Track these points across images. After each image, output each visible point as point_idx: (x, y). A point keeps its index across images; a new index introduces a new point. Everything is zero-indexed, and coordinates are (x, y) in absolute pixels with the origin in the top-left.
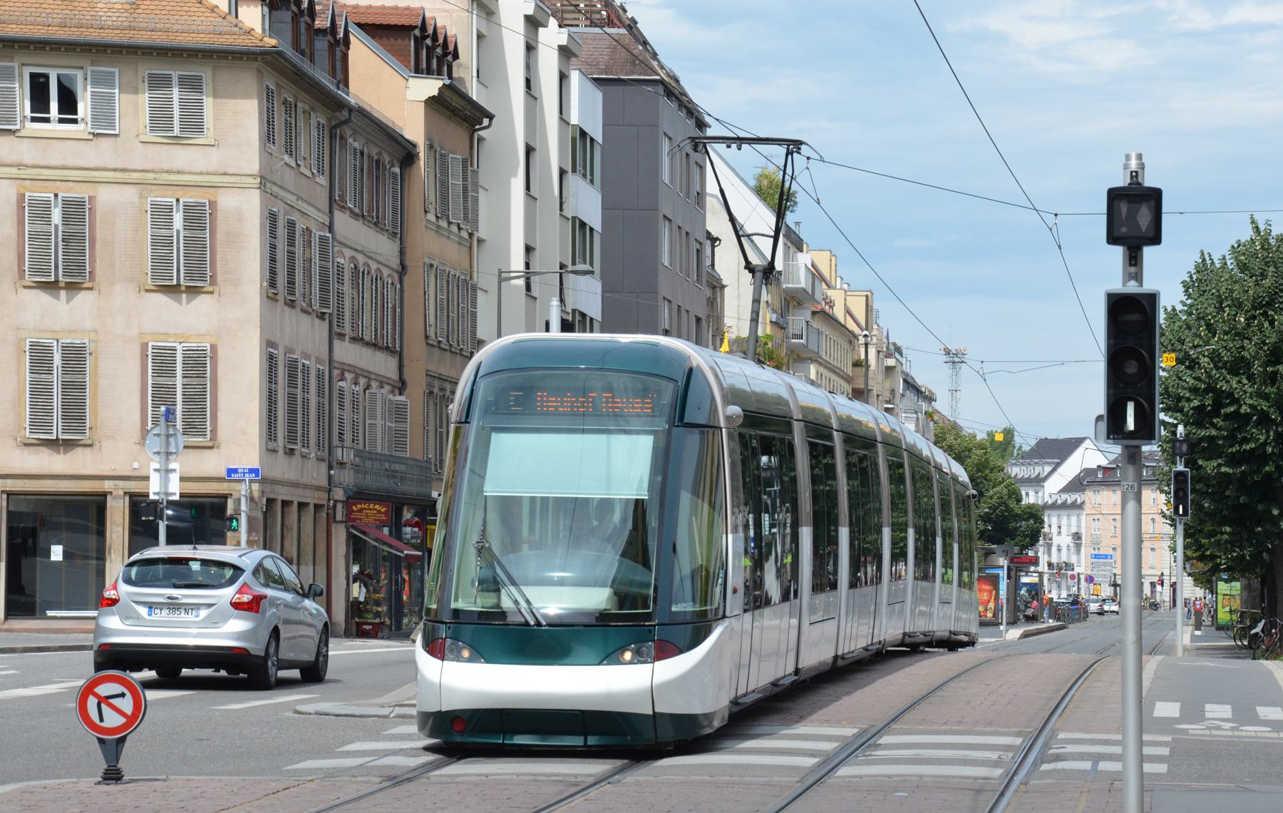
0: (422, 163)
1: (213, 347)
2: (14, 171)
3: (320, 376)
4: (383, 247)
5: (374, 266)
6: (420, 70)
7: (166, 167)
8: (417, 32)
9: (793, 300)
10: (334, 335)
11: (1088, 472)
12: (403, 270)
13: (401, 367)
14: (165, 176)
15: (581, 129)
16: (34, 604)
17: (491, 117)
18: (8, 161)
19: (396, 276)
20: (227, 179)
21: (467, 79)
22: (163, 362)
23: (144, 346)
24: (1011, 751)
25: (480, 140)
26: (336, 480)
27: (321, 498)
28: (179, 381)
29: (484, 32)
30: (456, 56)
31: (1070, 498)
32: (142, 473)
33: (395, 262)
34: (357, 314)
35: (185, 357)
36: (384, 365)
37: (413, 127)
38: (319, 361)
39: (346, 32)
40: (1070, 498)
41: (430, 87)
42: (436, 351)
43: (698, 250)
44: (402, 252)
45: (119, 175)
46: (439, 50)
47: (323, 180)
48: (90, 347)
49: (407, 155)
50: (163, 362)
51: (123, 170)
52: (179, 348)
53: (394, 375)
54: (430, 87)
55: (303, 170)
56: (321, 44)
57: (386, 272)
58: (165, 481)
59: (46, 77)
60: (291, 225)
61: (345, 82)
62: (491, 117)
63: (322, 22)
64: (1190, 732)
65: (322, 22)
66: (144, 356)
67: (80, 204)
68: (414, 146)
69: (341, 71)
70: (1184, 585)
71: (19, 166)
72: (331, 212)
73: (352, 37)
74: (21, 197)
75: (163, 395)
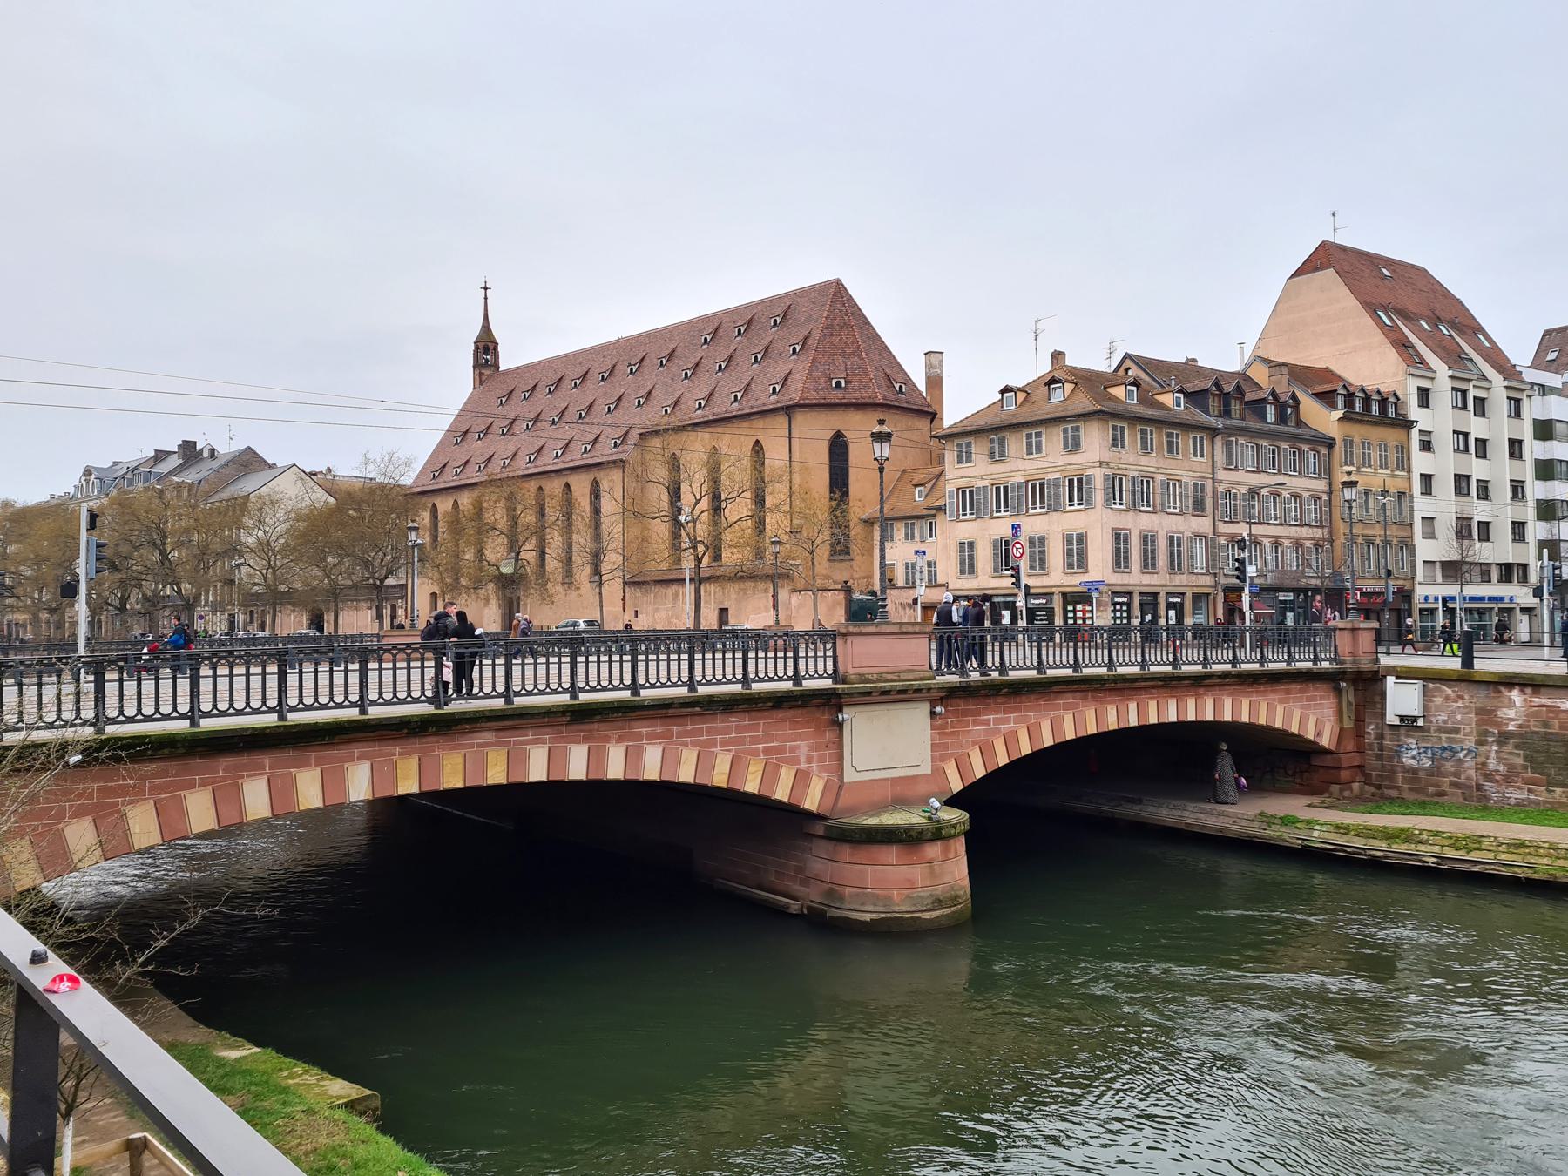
15: (1293, 276)
28: (1075, 547)
68: (1334, 439)
71: (1025, 470)
75: (1069, 554)
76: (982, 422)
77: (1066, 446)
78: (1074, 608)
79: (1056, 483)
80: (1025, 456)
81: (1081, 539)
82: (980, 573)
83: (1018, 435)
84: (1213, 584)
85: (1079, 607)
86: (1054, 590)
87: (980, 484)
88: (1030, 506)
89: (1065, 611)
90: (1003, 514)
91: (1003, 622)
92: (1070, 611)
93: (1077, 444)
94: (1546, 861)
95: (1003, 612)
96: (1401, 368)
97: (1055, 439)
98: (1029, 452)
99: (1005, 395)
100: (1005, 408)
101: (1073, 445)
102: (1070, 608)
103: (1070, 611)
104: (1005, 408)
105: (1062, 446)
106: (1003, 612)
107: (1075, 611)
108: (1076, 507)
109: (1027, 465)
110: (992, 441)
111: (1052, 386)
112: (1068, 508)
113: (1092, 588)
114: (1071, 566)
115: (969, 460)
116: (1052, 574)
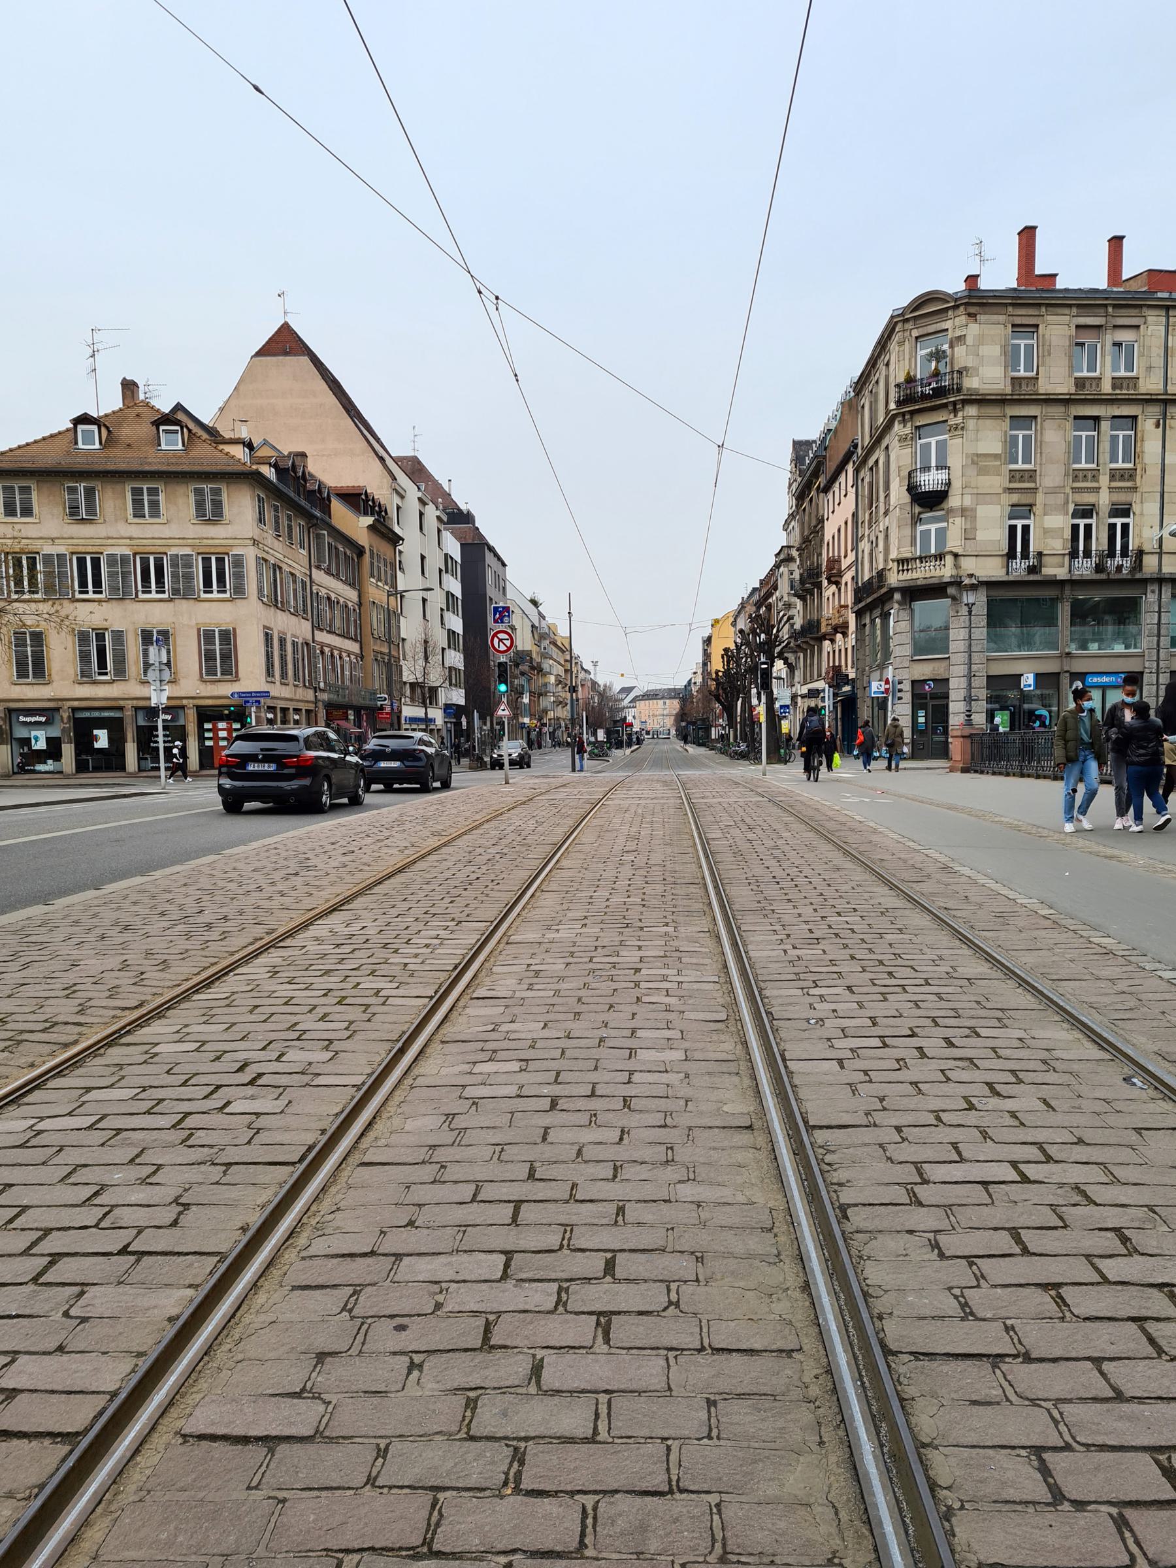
1: (234, 629)
2: (128, 542)
4: (352, 595)
5: (342, 600)
6: (366, 514)
7: (205, 536)
8: (363, 497)
9: (543, 637)
10: (316, 627)
11: (637, 697)
12: (360, 605)
13: (361, 648)
14: (205, 541)
15: (259, 353)
16: (995, 627)
17: (403, 540)
18: (125, 536)
19: (357, 607)
20: (237, 541)
22: (208, 637)
23: (199, 630)
25: (400, 552)
26: (319, 697)
27: (311, 707)
28: (218, 647)
29: (400, 505)
31: (632, 705)
32: (148, 695)
33: (356, 599)
34: (332, 619)
35: (220, 635)
36: (354, 647)
37: (363, 538)
40: (632, 705)
41: (369, 520)
42: (379, 641)
43: (398, 508)
45: (181, 541)
46: (377, 508)
48: (171, 631)
49: (360, 551)
50: (208, 637)
51: (184, 538)
52: (217, 630)
53: (358, 652)
54: (369, 520)
57: (350, 604)
58: (159, 697)
61: (330, 517)
62: (403, 540)
66: (199, 635)
68: (363, 547)
71: (131, 538)
75: (209, 655)
76: (49, 459)
77: (200, 511)
78: (215, 726)
79: (187, 560)
80: (131, 519)
81: (228, 637)
82: (54, 676)
83: (118, 487)
84: (313, 699)
85: (222, 725)
86: (185, 702)
87: (48, 549)
88: (140, 587)
89: (201, 731)
90: (215, 595)
91: (97, 745)
92: (209, 730)
93: (218, 511)
94: (766, 953)
95: (96, 732)
96: (385, 480)
97: (181, 501)
98: (138, 512)
99: (80, 427)
100: (163, 447)
101: (210, 512)
102: (208, 726)
103: (209, 730)
104: (81, 446)
105: (193, 511)
106: (96, 732)
107: (215, 730)
108: (154, 595)
109: (134, 531)
110: (73, 491)
111: (162, 428)
112: (203, 596)
113: (251, 700)
114: (211, 671)
115: (27, 511)
116: (182, 682)
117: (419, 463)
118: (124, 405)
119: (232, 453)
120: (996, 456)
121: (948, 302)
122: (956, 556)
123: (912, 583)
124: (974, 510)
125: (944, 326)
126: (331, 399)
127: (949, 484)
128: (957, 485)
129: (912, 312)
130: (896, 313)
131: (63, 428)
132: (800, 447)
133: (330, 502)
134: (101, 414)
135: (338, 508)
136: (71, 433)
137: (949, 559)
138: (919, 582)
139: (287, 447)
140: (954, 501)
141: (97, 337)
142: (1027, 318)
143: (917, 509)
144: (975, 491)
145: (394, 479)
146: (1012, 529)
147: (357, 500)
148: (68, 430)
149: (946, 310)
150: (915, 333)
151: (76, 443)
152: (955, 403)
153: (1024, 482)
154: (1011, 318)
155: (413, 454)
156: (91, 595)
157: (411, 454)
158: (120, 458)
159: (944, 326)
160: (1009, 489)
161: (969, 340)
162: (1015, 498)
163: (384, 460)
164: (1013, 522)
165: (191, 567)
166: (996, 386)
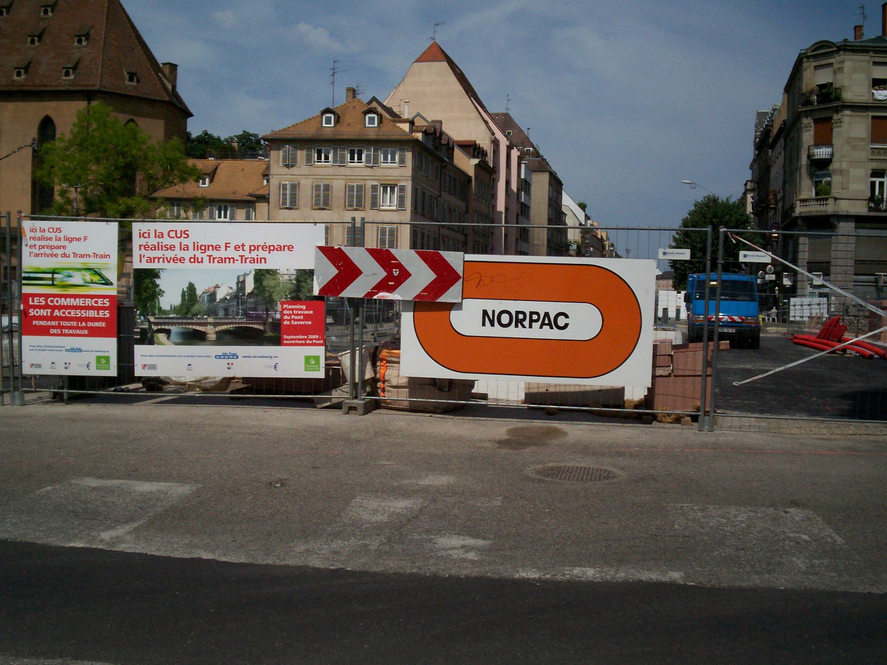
0: (473, 182)
2: (344, 177)
3: (435, 238)
6: (474, 157)
21: (489, 161)
24: (50, 309)
28: (387, 237)
30: (487, 156)
37: (471, 172)
38: (434, 233)
39: (453, 146)
41: (476, 161)
44: (467, 207)
47: (438, 182)
49: (469, 179)
54: (476, 161)
55: (430, 178)
56: (444, 148)
59: (31, 44)
60: (424, 194)
63: (444, 142)
64: (304, 307)
65: (444, 142)
67: (361, 186)
68: (471, 177)
69: (451, 158)
70: (356, 233)
71: (346, 176)
72: (440, 192)
73: (455, 148)
74: (346, 185)
104: (324, 125)
106: (54, 315)
117: (511, 118)
118: (347, 101)
119: (401, 127)
120: (863, 139)
121: (832, 47)
122: (836, 199)
123: (808, 214)
124: (848, 171)
125: (831, 61)
126: (458, 87)
127: (832, 155)
128: (837, 156)
129: (813, 51)
130: (803, 52)
131: (315, 115)
132: (761, 115)
133: (453, 150)
134: (335, 107)
135: (458, 154)
136: (319, 119)
137: (831, 201)
138: (813, 214)
139: (431, 116)
140: (834, 166)
141: (337, 65)
142: (882, 58)
143: (813, 169)
144: (848, 160)
145: (493, 134)
146: (873, 184)
147: (472, 149)
148: (318, 116)
149: (832, 52)
150: (814, 64)
151: (322, 123)
152: (836, 107)
153: (880, 155)
154: (872, 58)
155: (506, 112)
156: (388, 227)
157: (505, 112)
158: (347, 131)
159: (831, 61)
160: (871, 159)
161: (845, 70)
162: (875, 165)
163: (488, 123)
164: (873, 179)
165: (377, 192)
166: (861, 98)
